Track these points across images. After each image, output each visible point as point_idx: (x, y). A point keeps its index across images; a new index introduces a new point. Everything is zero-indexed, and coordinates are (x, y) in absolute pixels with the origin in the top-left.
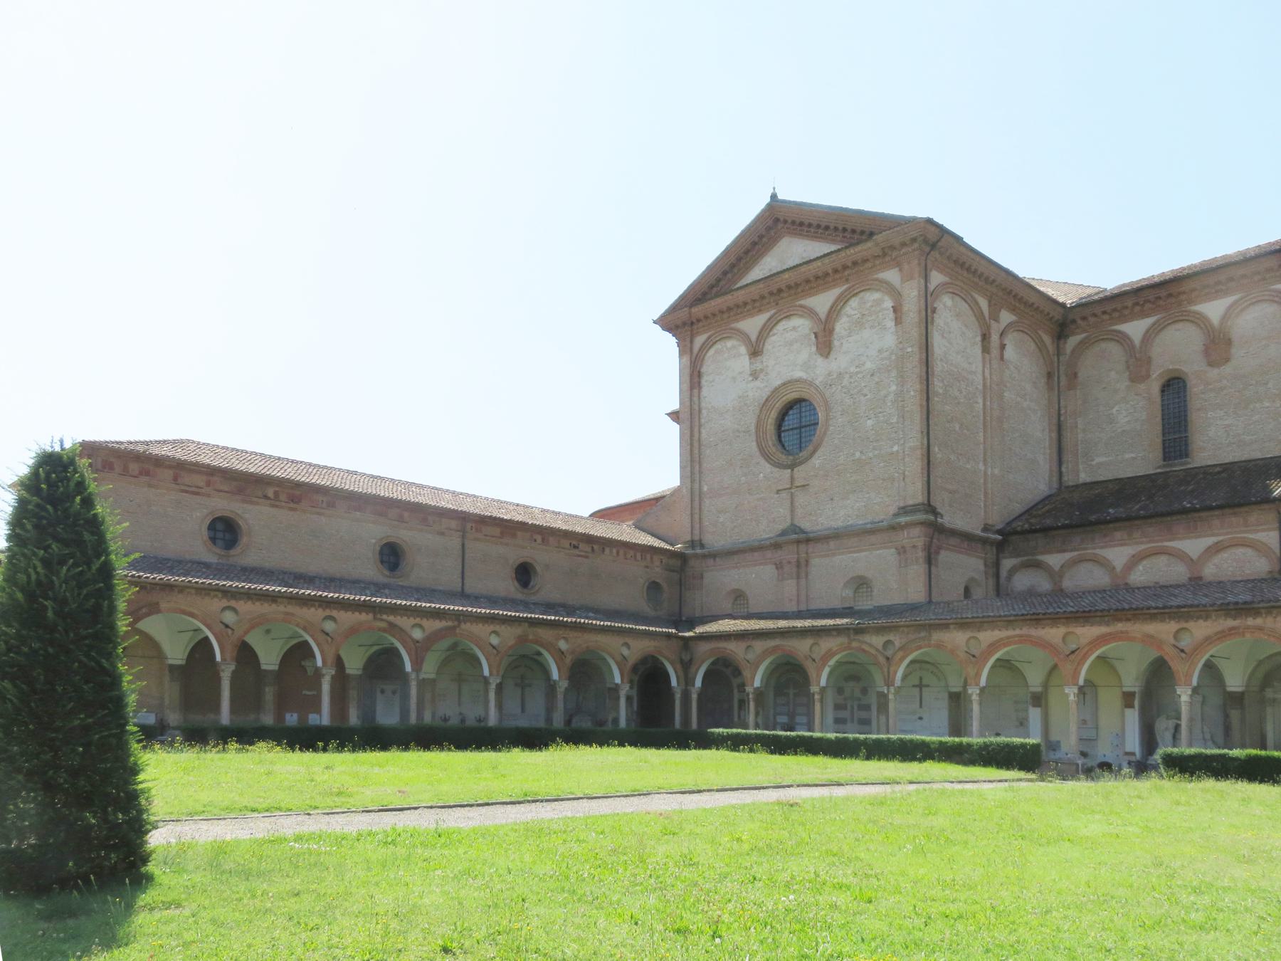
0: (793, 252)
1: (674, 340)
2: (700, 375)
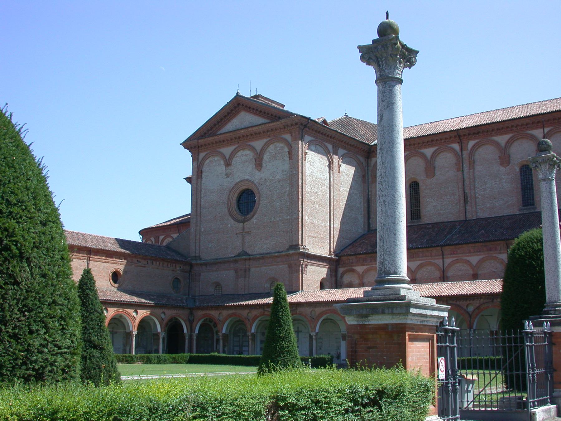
0: (244, 119)
1: (190, 153)
2: (201, 172)
